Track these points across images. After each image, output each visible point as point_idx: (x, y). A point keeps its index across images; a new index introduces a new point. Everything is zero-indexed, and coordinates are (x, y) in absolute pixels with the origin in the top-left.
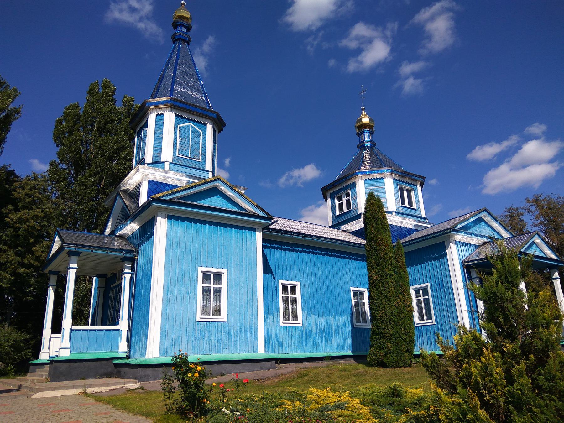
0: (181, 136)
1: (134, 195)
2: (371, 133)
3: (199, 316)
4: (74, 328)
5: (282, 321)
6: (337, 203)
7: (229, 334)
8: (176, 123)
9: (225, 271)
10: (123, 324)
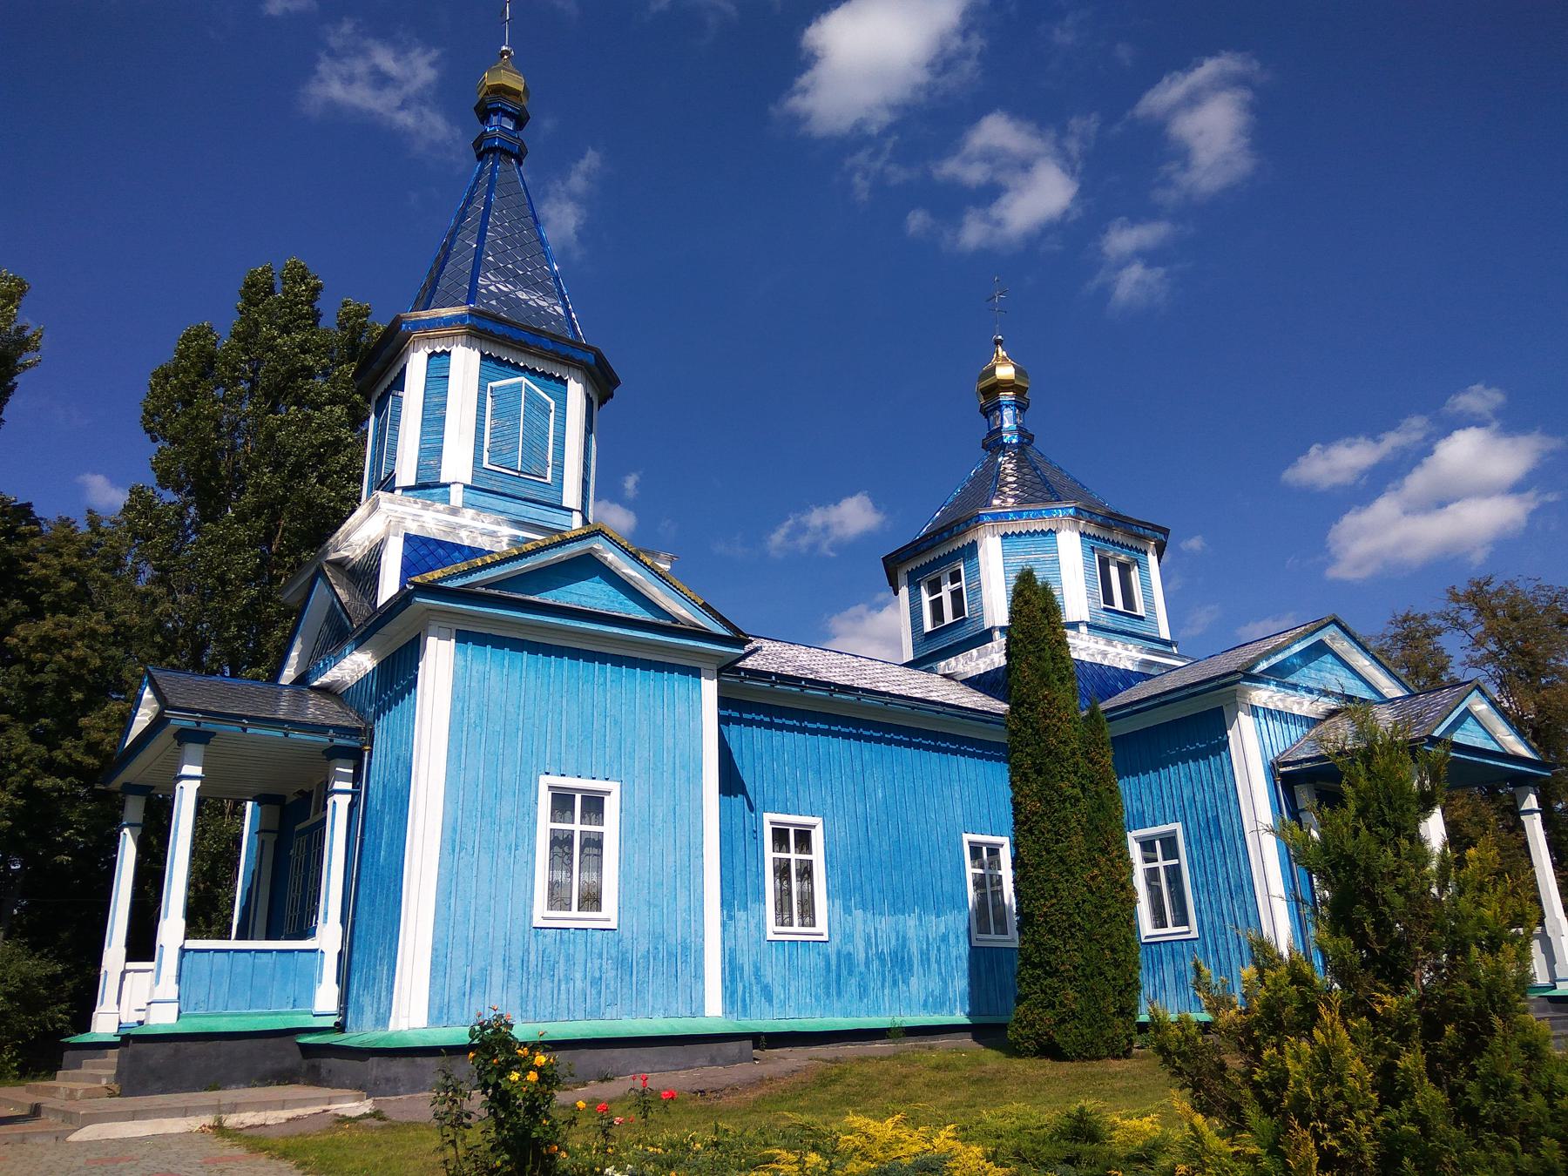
0: (496, 413)
1: (365, 574)
2: (1021, 407)
3: (541, 912)
4: (192, 944)
5: (771, 928)
6: (926, 599)
8: (484, 379)
9: (614, 786)
10: (328, 936)
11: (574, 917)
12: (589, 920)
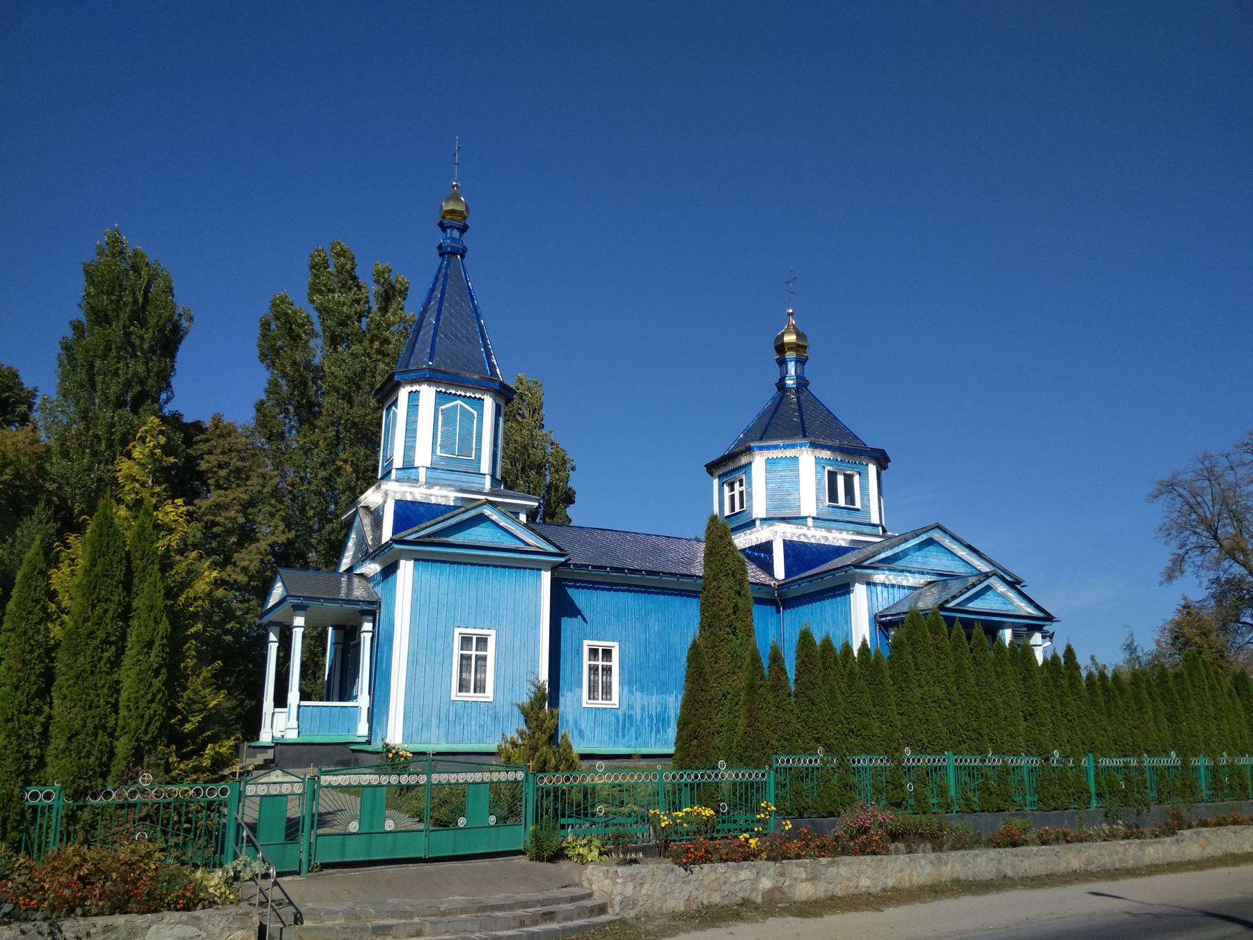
0: (445, 419)
1: (376, 516)
2: (801, 361)
3: (455, 694)
4: (303, 703)
5: (586, 702)
7: (495, 718)
8: (437, 405)
9: (493, 633)
10: (363, 700)
11: (471, 696)
12: (478, 697)
